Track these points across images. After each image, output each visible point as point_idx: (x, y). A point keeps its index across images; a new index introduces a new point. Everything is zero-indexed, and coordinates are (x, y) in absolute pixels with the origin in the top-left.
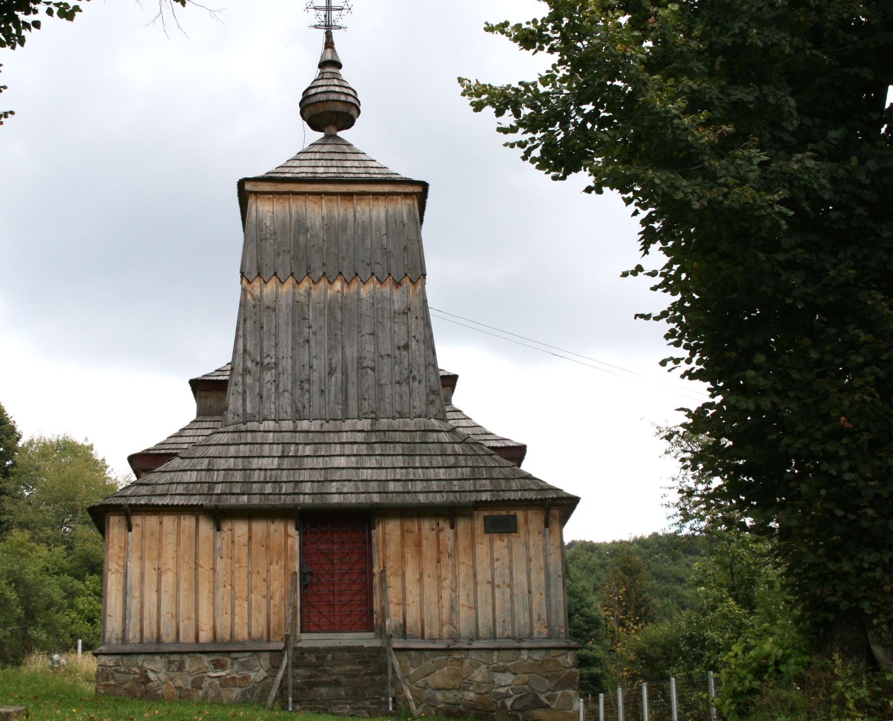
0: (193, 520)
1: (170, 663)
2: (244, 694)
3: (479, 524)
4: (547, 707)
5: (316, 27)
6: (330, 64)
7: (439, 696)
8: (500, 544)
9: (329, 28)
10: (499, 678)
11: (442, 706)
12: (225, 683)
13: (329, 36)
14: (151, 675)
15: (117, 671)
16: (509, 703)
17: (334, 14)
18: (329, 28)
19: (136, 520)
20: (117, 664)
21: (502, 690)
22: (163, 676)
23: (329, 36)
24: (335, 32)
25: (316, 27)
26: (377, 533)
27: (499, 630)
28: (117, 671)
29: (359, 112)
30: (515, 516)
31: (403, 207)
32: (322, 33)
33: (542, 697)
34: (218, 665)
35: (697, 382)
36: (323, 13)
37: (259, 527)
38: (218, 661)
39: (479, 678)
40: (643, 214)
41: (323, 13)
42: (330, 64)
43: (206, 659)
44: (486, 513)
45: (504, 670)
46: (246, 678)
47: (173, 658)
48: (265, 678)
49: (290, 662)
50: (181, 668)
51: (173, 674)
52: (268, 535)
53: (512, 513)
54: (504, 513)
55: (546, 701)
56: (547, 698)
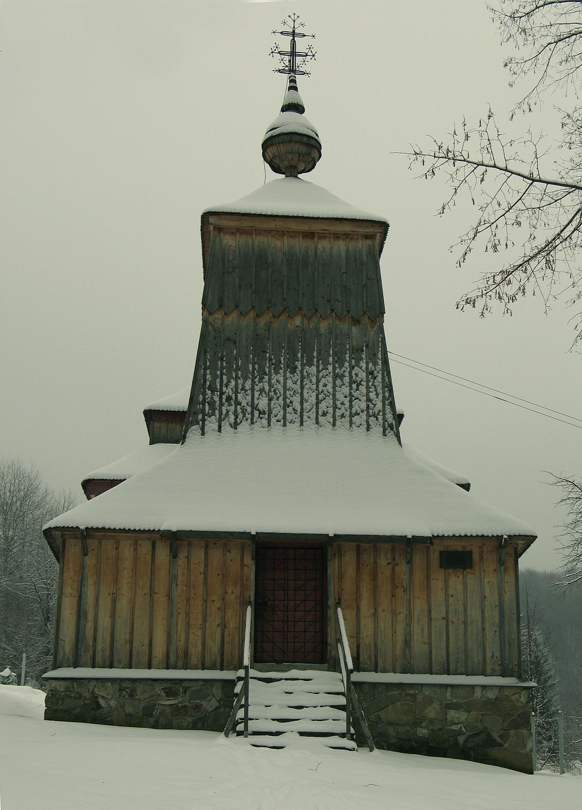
1: (121, 690)
5: (279, 71)
8: (456, 581)
10: (452, 714)
15: (67, 696)
16: (461, 739)
25: (279, 71)
32: (285, 77)
33: (495, 736)
36: (287, 58)
45: (456, 707)
46: (197, 707)
48: (217, 708)
55: (498, 740)
56: (501, 737)
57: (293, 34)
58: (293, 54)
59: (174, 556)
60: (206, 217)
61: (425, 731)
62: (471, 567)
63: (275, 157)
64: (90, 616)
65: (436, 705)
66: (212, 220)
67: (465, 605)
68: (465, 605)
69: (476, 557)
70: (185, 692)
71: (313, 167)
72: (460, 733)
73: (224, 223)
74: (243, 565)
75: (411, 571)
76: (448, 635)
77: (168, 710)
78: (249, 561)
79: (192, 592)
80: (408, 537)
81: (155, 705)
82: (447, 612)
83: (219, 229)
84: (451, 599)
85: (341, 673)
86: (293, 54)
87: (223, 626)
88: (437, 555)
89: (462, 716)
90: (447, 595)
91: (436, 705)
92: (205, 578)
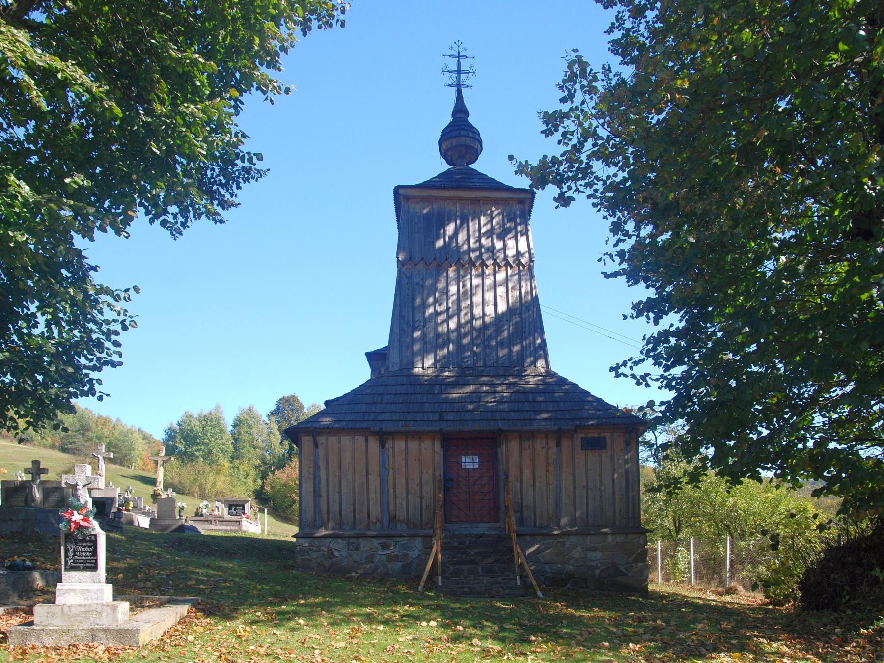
0: (364, 439)
1: (349, 544)
2: (403, 566)
3: (578, 443)
4: (625, 574)
5: (449, 85)
6: (460, 111)
7: (547, 568)
8: (593, 457)
9: (459, 87)
10: (591, 555)
11: (549, 574)
12: (391, 559)
13: (459, 93)
14: (336, 554)
15: (310, 549)
16: (597, 572)
17: (463, 76)
18: (459, 87)
19: (321, 440)
20: (311, 545)
21: (593, 564)
22: (344, 554)
23: (459, 93)
24: (464, 91)
25: (449, 85)
26: (502, 450)
27: (591, 521)
28: (310, 549)
29: (480, 142)
30: (604, 438)
31: (530, 196)
32: (454, 89)
33: (622, 568)
34: (385, 546)
35: (93, 264)
36: (454, 75)
37: (413, 445)
38: (384, 543)
39: (577, 556)
40: (94, 375)
41: (454, 75)
42: (460, 111)
43: (376, 542)
44: (583, 435)
45: (595, 549)
46: (405, 556)
47: (351, 541)
48: (420, 556)
49: (439, 548)
50: (357, 548)
51: (352, 552)
52: (420, 452)
53: (602, 435)
54: (596, 435)
55: (624, 571)
56: (625, 568)
57: (459, 56)
58: (459, 72)
59: (382, 445)
60: (397, 189)
61: (571, 567)
62: (605, 448)
63: (448, 150)
64: (324, 494)
65: (579, 548)
66: (401, 191)
67: (600, 476)
68: (600, 476)
69: (608, 441)
70: (395, 545)
71: (477, 159)
72: (597, 567)
73: (410, 192)
74: (434, 451)
75: (560, 452)
76: (587, 499)
77: (384, 558)
78: (437, 446)
79: (397, 473)
80: (653, 362)
81: (373, 555)
82: (587, 482)
83: (408, 198)
84: (590, 472)
85: (93, 498)
86: (459, 72)
87: (464, 286)
88: (579, 439)
89: (598, 555)
90: (587, 468)
91: (579, 548)
92: (406, 463)
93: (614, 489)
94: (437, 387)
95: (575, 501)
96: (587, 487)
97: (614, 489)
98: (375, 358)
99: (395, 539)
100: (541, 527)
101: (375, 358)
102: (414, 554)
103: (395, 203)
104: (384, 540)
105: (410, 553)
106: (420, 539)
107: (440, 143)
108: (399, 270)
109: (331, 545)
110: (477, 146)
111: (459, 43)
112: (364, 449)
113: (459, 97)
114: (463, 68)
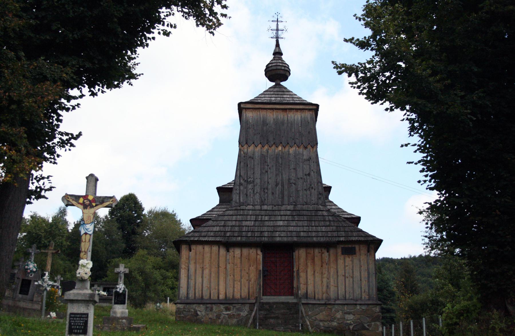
0: (217, 247)
1: (207, 308)
2: (238, 321)
3: (339, 251)
4: (368, 329)
6: (278, 54)
9: (277, 38)
10: (347, 316)
11: (322, 328)
12: (230, 316)
14: (199, 313)
16: (351, 327)
18: (277, 38)
19: (193, 247)
20: (184, 308)
21: (348, 322)
22: (203, 313)
23: (277, 42)
24: (280, 40)
26: (296, 254)
27: (347, 296)
29: (290, 74)
31: (308, 115)
32: (275, 40)
33: (366, 325)
34: (227, 309)
36: (275, 32)
37: (245, 251)
38: (227, 307)
39: (339, 316)
42: (278, 54)
43: (222, 307)
45: (349, 313)
46: (239, 315)
48: (247, 315)
51: (208, 312)
53: (354, 246)
55: (367, 327)
56: (368, 325)
62: (355, 254)
65: (340, 312)
72: (351, 324)
86: (277, 30)
93: (361, 277)
94: (260, 217)
95: (338, 284)
96: (345, 276)
97: (361, 277)
98: (328, 189)
99: (233, 305)
100: (319, 300)
101: (328, 189)
102: (244, 314)
103: (239, 109)
104: (227, 305)
105: (242, 313)
106: (248, 305)
107: (265, 74)
108: (240, 150)
109: (196, 308)
110: (288, 74)
111: (277, 14)
112: (217, 252)
113: (278, 45)
114: (280, 28)
